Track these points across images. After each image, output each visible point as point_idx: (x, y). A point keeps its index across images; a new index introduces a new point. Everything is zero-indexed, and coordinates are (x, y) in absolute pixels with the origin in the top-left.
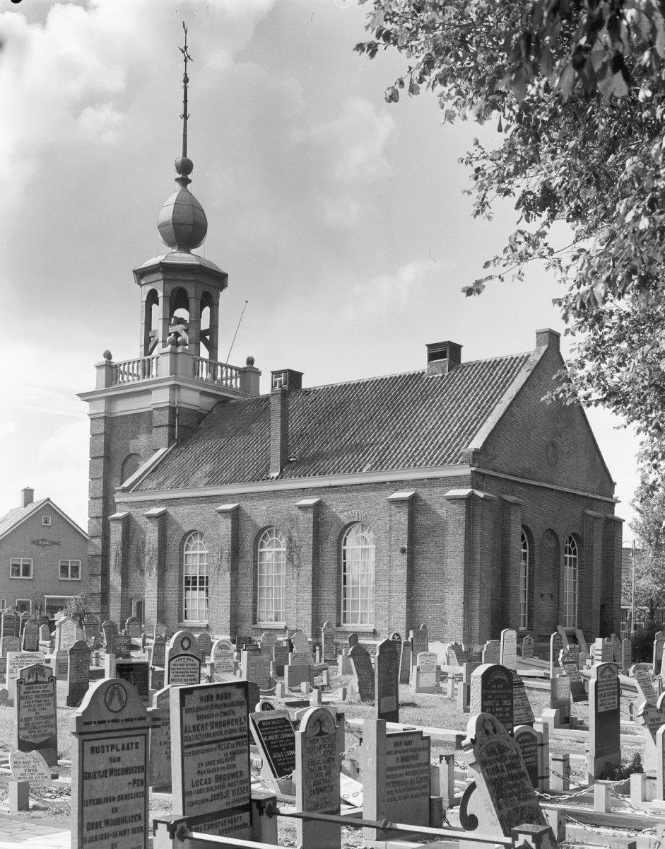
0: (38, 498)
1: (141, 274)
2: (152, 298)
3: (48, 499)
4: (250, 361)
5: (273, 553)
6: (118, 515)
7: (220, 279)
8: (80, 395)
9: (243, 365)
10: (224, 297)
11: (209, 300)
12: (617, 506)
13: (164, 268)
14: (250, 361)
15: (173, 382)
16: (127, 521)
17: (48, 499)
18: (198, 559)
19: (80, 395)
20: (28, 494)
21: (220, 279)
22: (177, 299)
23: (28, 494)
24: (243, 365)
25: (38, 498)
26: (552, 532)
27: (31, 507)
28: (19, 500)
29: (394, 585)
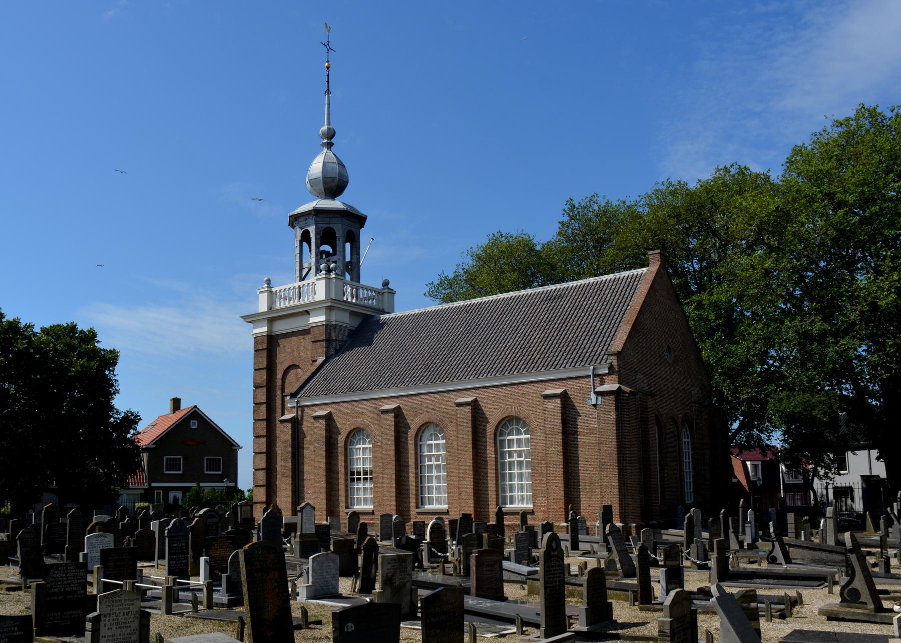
0: (185, 405)
1: (294, 220)
2: (306, 237)
3: (196, 407)
4: (386, 284)
5: (518, 444)
6: (287, 416)
7: (361, 220)
8: (244, 317)
9: (379, 286)
10: (365, 235)
11: (353, 239)
12: (121, 374)
13: (317, 212)
14: (386, 284)
15: (329, 304)
16: (296, 423)
17: (196, 407)
18: (363, 456)
19: (244, 317)
20: (176, 403)
21: (361, 220)
22: (327, 236)
23: (176, 403)
24: (379, 286)
25: (185, 405)
26: (673, 419)
27: (179, 415)
28: (168, 408)
29: (551, 471)
